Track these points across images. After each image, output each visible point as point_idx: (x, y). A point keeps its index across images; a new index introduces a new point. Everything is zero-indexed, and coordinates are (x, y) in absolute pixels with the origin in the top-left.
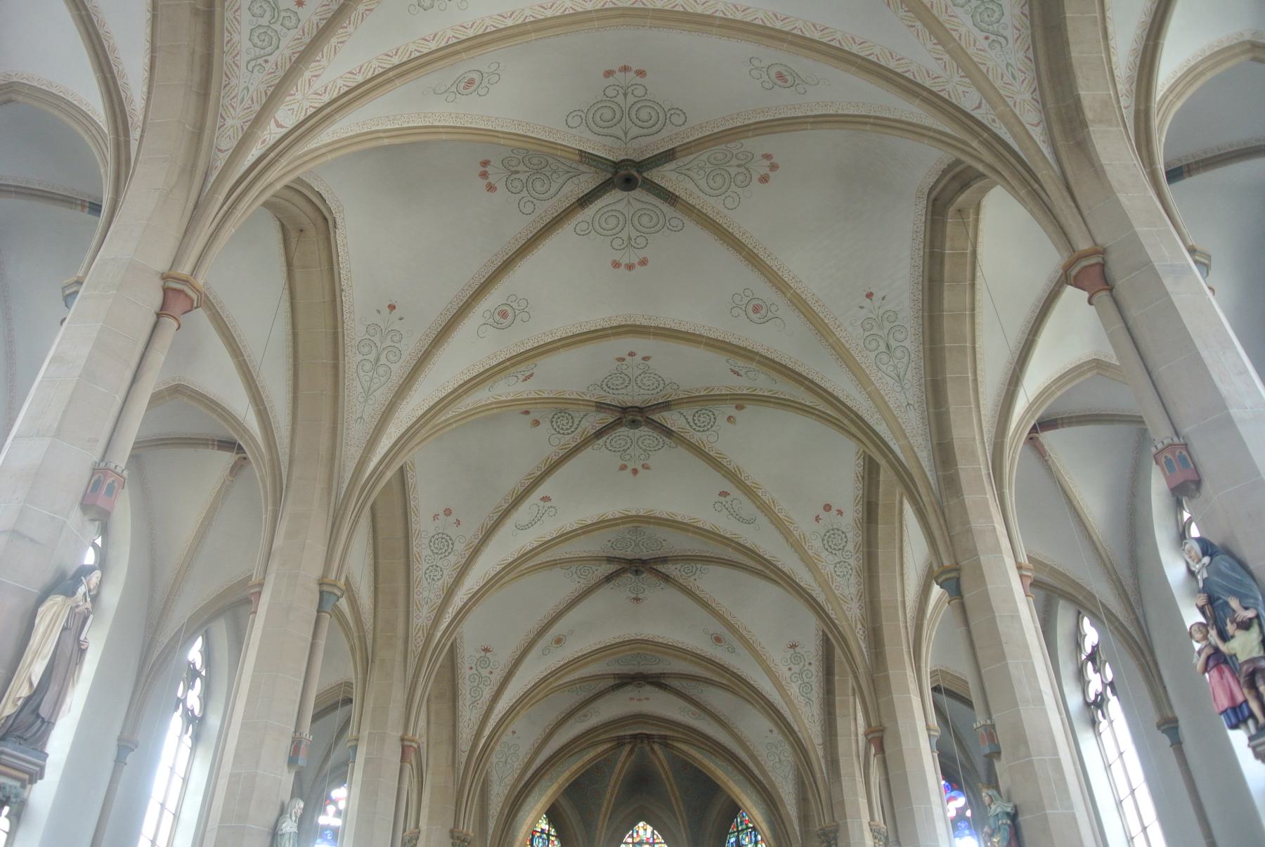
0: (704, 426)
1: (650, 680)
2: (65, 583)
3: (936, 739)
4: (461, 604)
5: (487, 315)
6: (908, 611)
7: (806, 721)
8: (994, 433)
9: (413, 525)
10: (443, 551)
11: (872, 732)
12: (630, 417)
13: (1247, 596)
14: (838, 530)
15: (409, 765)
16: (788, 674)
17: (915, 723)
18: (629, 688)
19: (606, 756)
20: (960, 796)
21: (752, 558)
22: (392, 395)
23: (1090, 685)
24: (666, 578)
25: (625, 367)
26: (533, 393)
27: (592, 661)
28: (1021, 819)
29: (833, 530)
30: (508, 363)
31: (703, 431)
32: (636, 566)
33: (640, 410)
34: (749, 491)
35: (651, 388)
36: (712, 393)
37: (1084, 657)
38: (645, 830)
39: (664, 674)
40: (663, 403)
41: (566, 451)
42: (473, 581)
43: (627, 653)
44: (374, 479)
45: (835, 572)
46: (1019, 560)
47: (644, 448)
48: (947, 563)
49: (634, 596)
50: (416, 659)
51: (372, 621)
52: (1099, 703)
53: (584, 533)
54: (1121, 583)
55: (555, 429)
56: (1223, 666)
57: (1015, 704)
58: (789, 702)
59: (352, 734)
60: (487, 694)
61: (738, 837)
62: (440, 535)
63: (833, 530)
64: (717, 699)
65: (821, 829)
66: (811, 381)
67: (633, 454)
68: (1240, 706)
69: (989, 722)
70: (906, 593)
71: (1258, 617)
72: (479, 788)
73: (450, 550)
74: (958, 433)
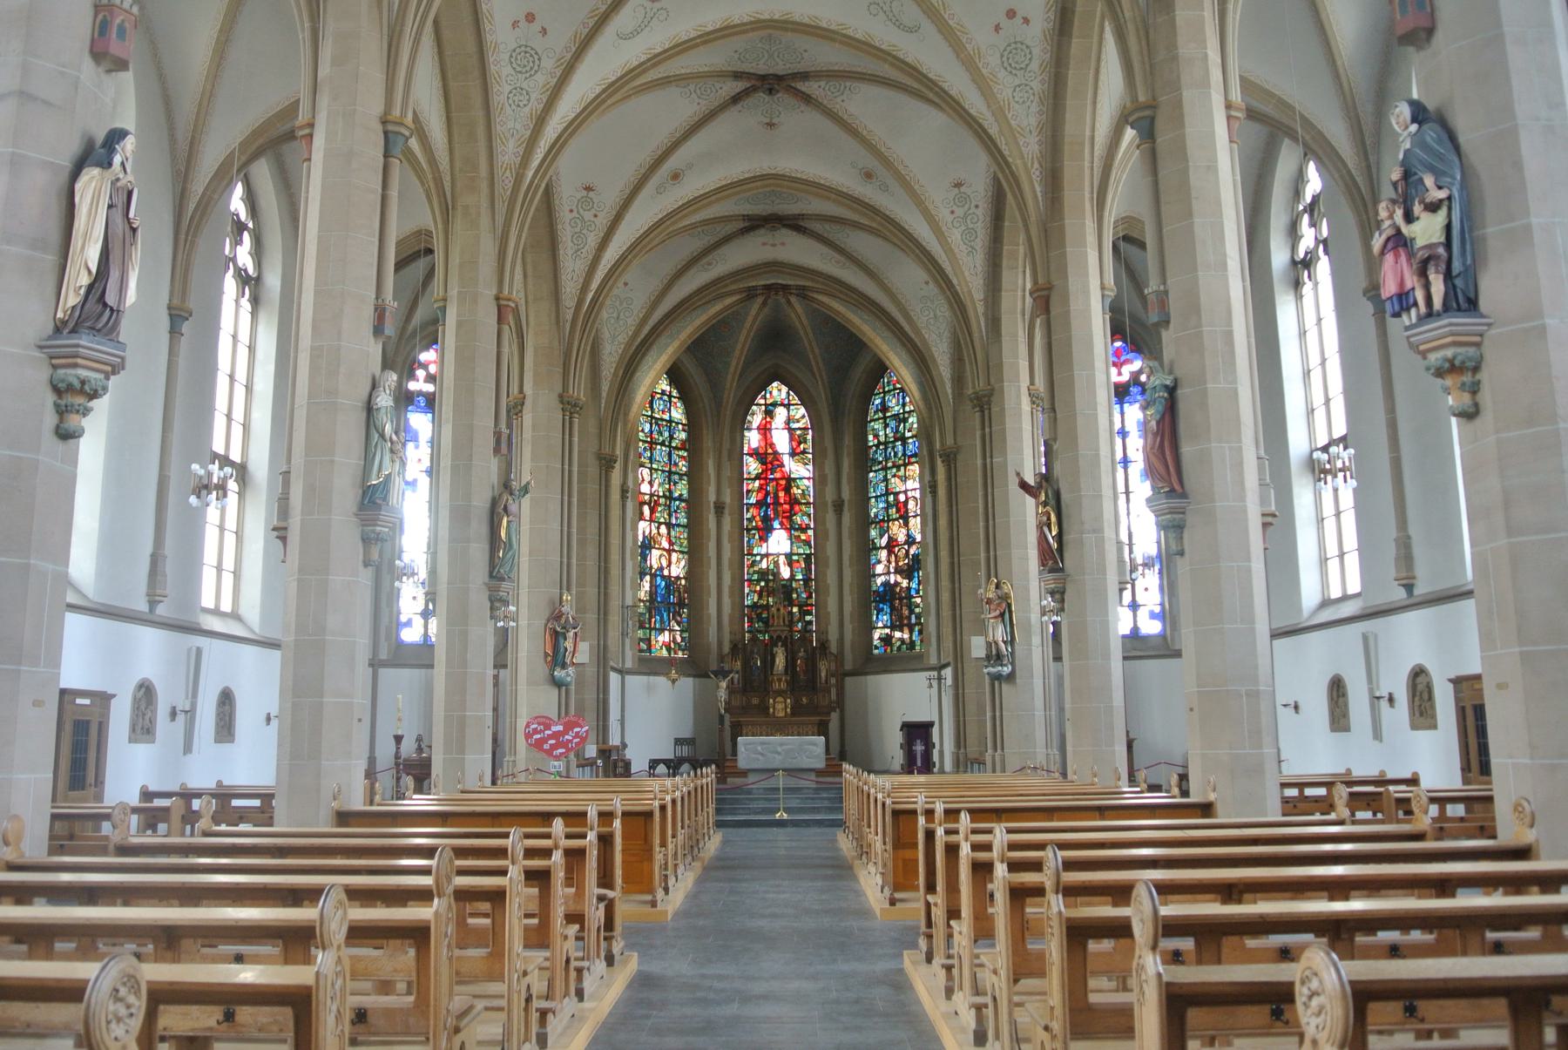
1: (786, 222)
2: (97, 152)
3: (1110, 300)
6: (1096, 149)
7: (966, 274)
9: (488, 35)
10: (528, 68)
11: (1038, 290)
13: (1444, 173)
15: (507, 327)
16: (950, 218)
17: (1088, 282)
18: (762, 231)
19: (735, 309)
20: (1136, 358)
21: (911, 75)
24: (807, 99)
27: (718, 200)
28: (1179, 392)
29: (1015, 43)
32: (770, 84)
37: (1301, 208)
38: (780, 390)
42: (567, 107)
43: (760, 190)
48: (1142, 98)
49: (767, 120)
50: (506, 204)
51: (448, 158)
52: (1308, 263)
53: (705, 42)
54: (1359, 121)
56: (1401, 250)
57: (1194, 268)
58: (949, 251)
59: (438, 294)
60: (592, 240)
61: (884, 398)
62: (523, 49)
63: (1015, 43)
64: (863, 244)
65: (974, 393)
68: (1408, 293)
69: (1162, 288)
70: (1097, 125)
71: (1449, 198)
72: (589, 349)
73: (536, 68)
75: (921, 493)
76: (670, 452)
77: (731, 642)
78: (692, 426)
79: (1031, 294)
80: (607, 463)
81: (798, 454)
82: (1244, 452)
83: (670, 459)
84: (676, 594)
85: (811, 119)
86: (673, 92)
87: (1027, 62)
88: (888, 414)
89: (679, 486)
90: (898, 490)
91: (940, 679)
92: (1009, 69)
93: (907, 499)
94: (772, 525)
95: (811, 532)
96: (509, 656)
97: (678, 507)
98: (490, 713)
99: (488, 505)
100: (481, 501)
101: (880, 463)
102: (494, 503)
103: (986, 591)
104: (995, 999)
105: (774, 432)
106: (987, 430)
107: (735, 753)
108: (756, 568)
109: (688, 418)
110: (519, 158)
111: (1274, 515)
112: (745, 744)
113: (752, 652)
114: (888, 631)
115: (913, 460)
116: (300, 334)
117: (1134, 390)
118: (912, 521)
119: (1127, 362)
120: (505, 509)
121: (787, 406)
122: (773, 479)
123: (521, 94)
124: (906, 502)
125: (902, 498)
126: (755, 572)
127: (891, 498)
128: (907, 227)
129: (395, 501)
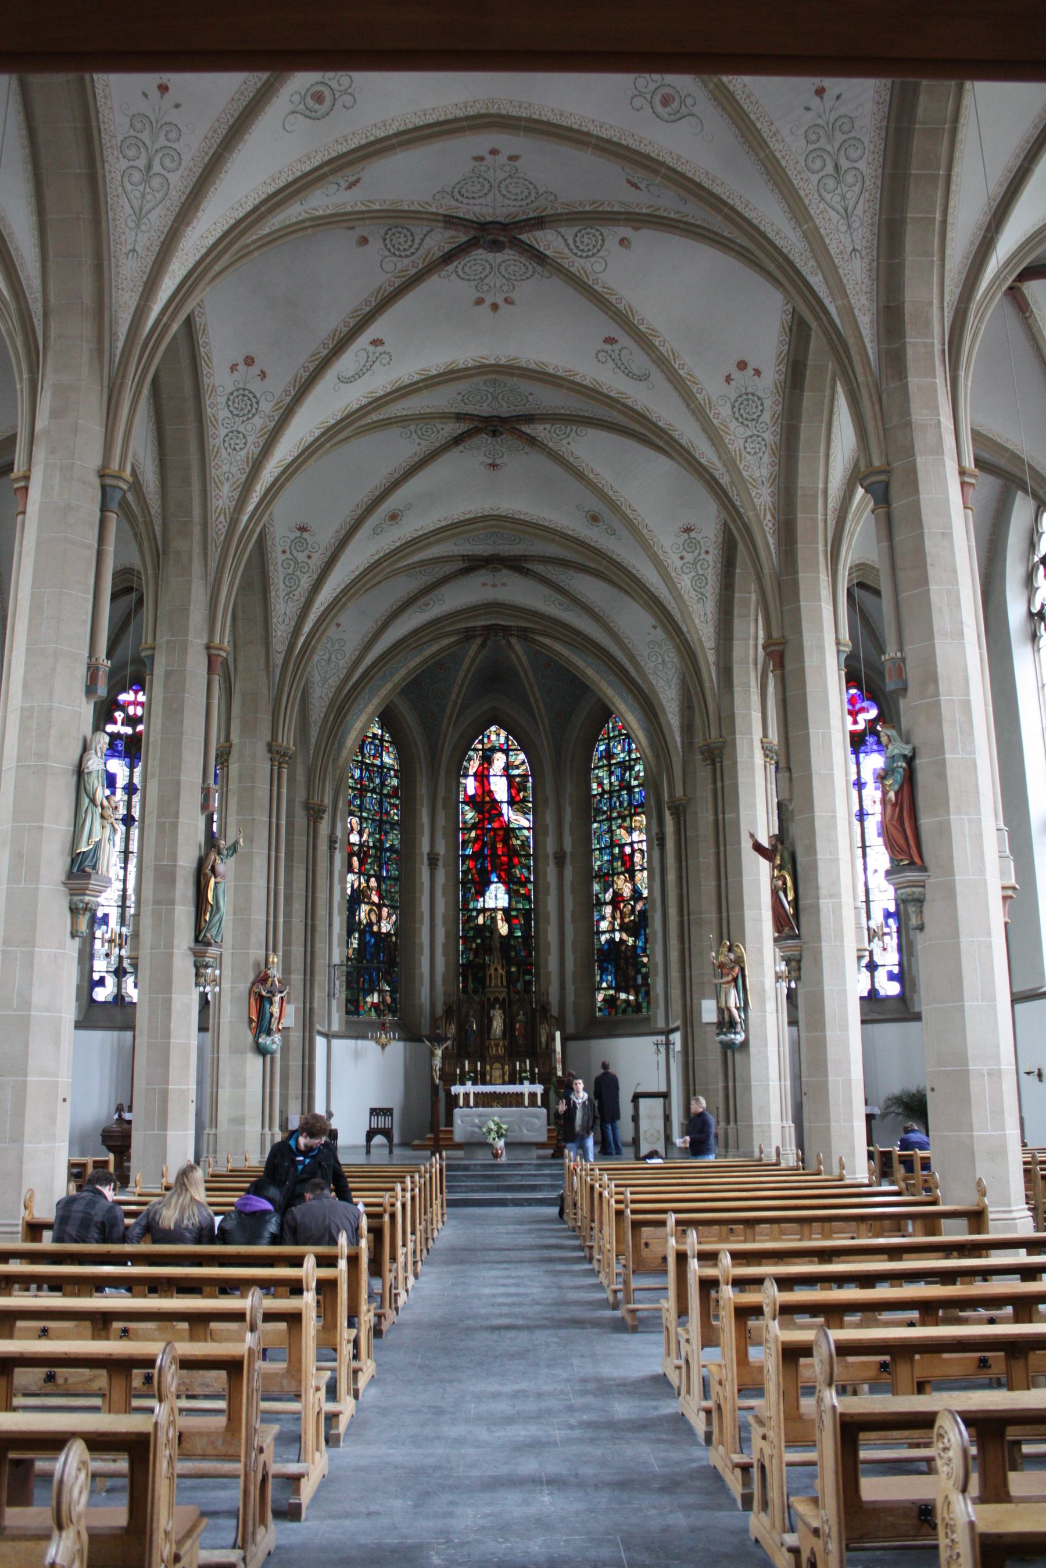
0: (589, 250)
4: (271, 480)
5: (296, 98)
6: (830, 500)
7: (697, 621)
8: (957, 295)
9: (205, 379)
10: (246, 412)
12: (490, 237)
14: (753, 395)
16: (679, 563)
18: (482, 572)
19: (452, 649)
20: (871, 706)
21: (642, 425)
22: (172, 218)
23: (1039, 592)
24: (532, 441)
25: (483, 168)
26: (359, 203)
28: (918, 762)
29: (747, 394)
30: (326, 169)
31: (587, 257)
33: (504, 227)
34: (644, 341)
35: (519, 197)
36: (601, 209)
37: (1036, 559)
38: (498, 735)
39: (526, 556)
40: (534, 218)
41: (404, 279)
44: (156, 335)
45: (745, 448)
46: (963, 464)
47: (507, 276)
48: (877, 463)
49: (490, 461)
50: (219, 550)
53: (426, 387)
55: (389, 250)
58: (678, 597)
59: (146, 643)
60: (305, 582)
61: (608, 745)
62: (241, 392)
66: (732, 208)
67: (492, 284)
69: (899, 655)
70: (831, 477)
72: (299, 695)
73: (254, 411)
74: (912, 295)
75: (647, 846)
76: (381, 800)
77: (445, 1003)
78: (405, 771)
79: (764, 648)
80: (314, 813)
81: (517, 803)
82: (983, 825)
83: (381, 807)
84: (387, 952)
85: (536, 460)
86: (395, 431)
87: (759, 413)
88: (614, 761)
89: (391, 836)
90: (623, 842)
91: (668, 1044)
92: (740, 420)
93: (633, 851)
94: (490, 879)
95: (530, 886)
96: (211, 1021)
97: (389, 858)
98: (193, 1086)
99: (194, 865)
100: (187, 860)
101: (605, 812)
102: (201, 862)
103: (718, 954)
104: (687, 1362)
105: (492, 779)
106: (719, 784)
107: (450, 1122)
108: (472, 925)
109: (400, 764)
110: (234, 503)
111: (1014, 888)
112: (462, 1117)
113: (467, 1015)
114: (612, 992)
115: (640, 810)
116: (10, 693)
117: (870, 740)
118: (638, 876)
119: (862, 710)
120: (213, 870)
121: (506, 752)
122: (492, 829)
123: (238, 438)
124: (632, 855)
125: (628, 850)
126: (471, 928)
127: (616, 850)
128: (634, 572)
129: (105, 869)
